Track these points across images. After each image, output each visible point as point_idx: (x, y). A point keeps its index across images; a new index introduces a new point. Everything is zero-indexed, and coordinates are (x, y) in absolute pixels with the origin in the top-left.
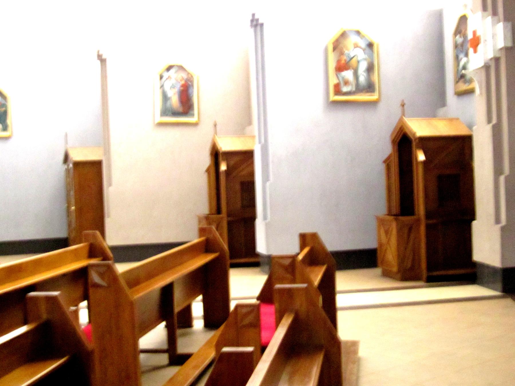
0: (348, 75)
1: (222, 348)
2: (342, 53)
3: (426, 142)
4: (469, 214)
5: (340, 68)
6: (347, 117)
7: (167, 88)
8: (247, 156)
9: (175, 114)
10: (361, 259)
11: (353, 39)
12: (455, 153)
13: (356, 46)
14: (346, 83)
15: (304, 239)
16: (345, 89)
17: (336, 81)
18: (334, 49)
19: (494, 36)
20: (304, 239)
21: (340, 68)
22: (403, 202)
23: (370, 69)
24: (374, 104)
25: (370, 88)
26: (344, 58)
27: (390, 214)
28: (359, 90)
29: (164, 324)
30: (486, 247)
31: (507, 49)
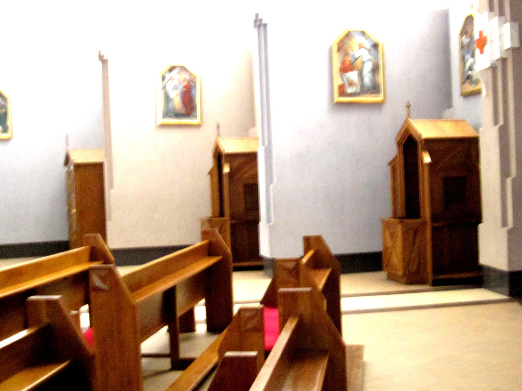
0: (353, 76)
1: (225, 353)
2: (346, 54)
3: (431, 144)
4: (475, 217)
5: (345, 69)
6: (352, 119)
7: (169, 89)
8: (251, 158)
9: (178, 115)
10: (366, 263)
11: (357, 40)
12: (461, 154)
13: (361, 47)
14: (351, 84)
15: (309, 242)
16: (350, 90)
17: (340, 82)
18: (339, 49)
19: (501, 36)
20: (309, 242)
21: (345, 69)
22: (408, 205)
23: (375, 70)
24: (379, 105)
25: (375, 89)
26: (349, 59)
27: (395, 216)
28: (364, 91)
29: (166, 328)
30: (493, 250)
31: (514, 50)
